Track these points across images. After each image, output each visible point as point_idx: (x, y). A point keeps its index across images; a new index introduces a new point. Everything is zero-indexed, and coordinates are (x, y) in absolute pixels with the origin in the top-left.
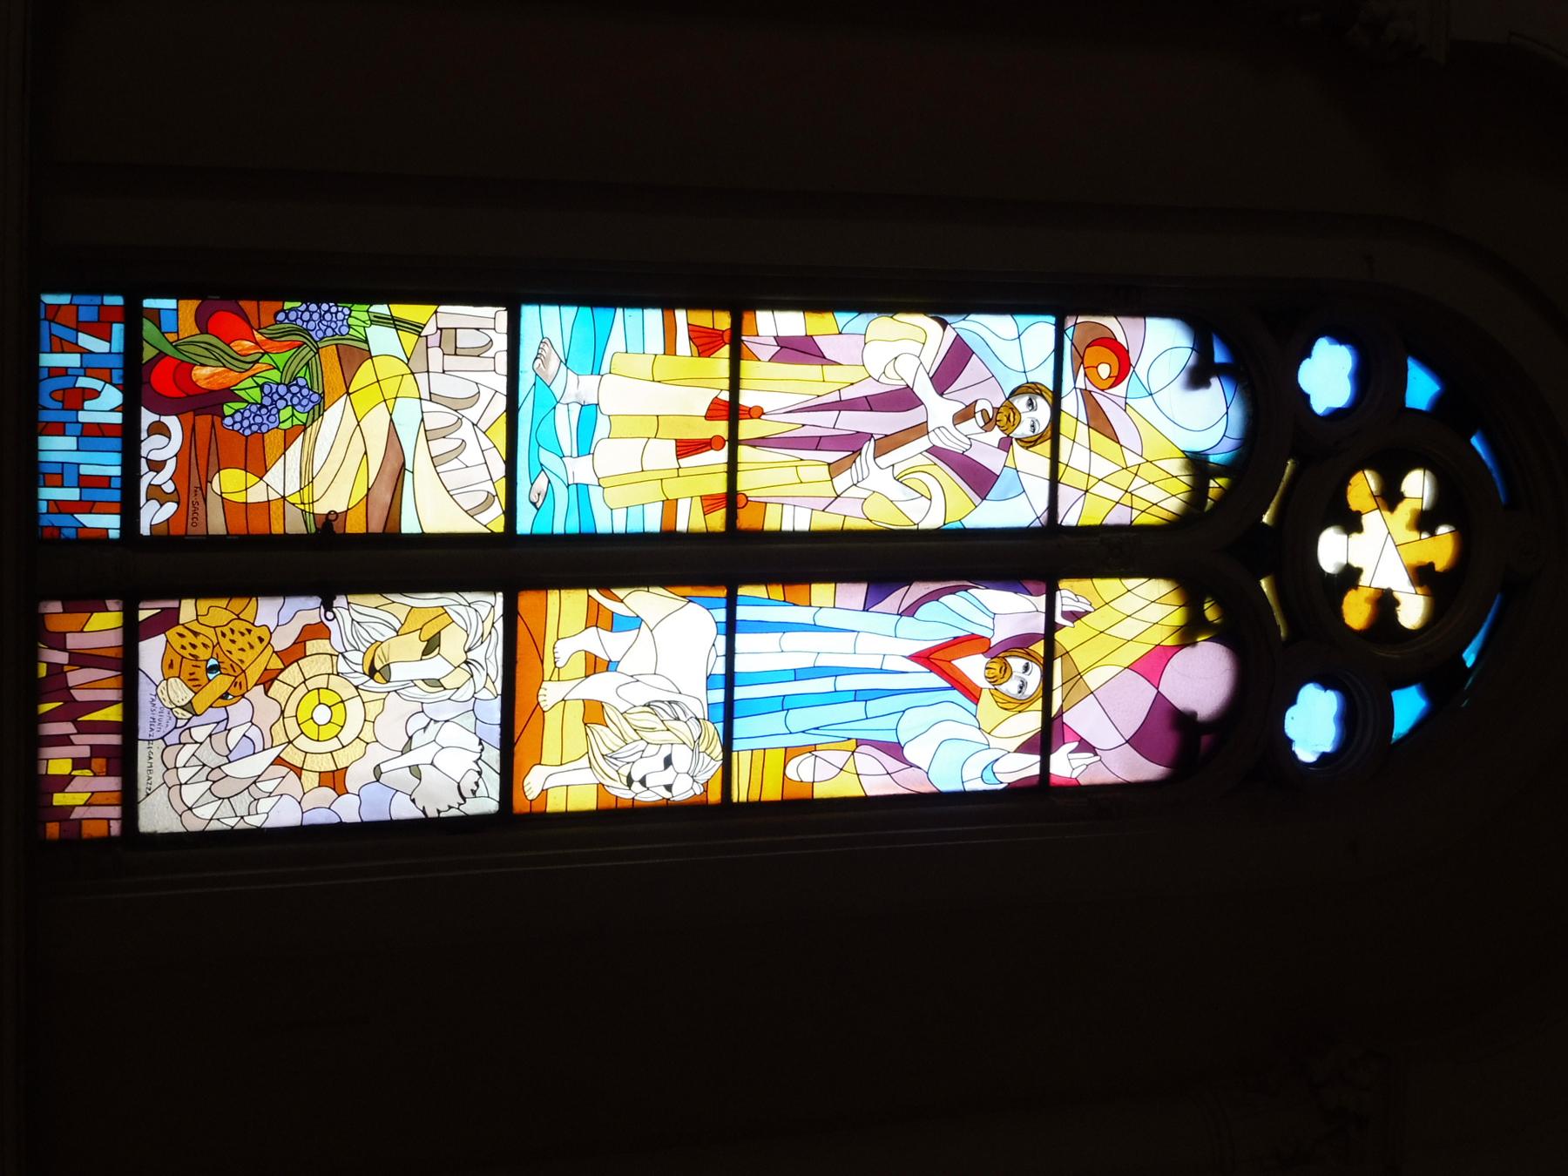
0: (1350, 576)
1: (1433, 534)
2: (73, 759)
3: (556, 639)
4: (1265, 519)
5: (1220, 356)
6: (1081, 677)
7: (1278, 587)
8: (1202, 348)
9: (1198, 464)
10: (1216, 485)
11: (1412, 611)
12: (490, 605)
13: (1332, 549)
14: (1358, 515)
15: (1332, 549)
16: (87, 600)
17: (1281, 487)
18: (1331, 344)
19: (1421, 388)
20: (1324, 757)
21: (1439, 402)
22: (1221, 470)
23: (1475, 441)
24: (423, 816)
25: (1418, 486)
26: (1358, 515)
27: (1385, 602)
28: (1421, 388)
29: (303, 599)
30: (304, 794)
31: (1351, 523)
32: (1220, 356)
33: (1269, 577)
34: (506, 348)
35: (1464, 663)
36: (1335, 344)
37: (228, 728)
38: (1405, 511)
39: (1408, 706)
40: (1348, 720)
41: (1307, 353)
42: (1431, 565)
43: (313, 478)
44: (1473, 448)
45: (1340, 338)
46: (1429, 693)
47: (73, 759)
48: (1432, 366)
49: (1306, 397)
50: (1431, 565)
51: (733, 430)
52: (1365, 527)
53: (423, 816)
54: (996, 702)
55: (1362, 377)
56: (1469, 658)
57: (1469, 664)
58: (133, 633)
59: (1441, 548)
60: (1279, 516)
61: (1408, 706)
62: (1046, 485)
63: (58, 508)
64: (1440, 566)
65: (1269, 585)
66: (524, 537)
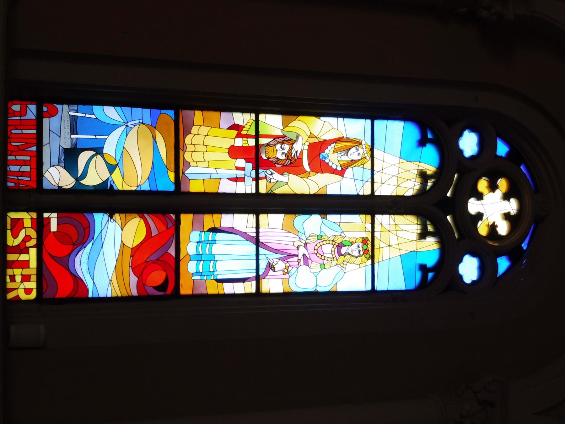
0: (479, 216)
1: (509, 200)
2: (29, 268)
4: (449, 194)
5: (430, 136)
7: (454, 219)
8: (424, 227)
9: (423, 175)
10: (430, 275)
11: (503, 229)
12: (171, 113)
13: (473, 206)
16: (25, 100)
18: (469, 132)
19: (502, 149)
20: (473, 282)
21: (508, 154)
22: (431, 177)
23: (522, 167)
25: (502, 184)
27: (493, 187)
28: (502, 149)
31: (480, 196)
32: (430, 136)
33: (450, 215)
38: (499, 193)
39: (503, 264)
40: (482, 268)
41: (461, 261)
43: (110, 283)
46: (510, 259)
47: (29, 268)
48: (507, 142)
50: (509, 213)
51: (257, 142)
55: (481, 144)
56: (524, 246)
57: (525, 248)
58: (40, 116)
59: (512, 206)
60: (454, 193)
61: (503, 264)
62: (370, 171)
65: (450, 218)
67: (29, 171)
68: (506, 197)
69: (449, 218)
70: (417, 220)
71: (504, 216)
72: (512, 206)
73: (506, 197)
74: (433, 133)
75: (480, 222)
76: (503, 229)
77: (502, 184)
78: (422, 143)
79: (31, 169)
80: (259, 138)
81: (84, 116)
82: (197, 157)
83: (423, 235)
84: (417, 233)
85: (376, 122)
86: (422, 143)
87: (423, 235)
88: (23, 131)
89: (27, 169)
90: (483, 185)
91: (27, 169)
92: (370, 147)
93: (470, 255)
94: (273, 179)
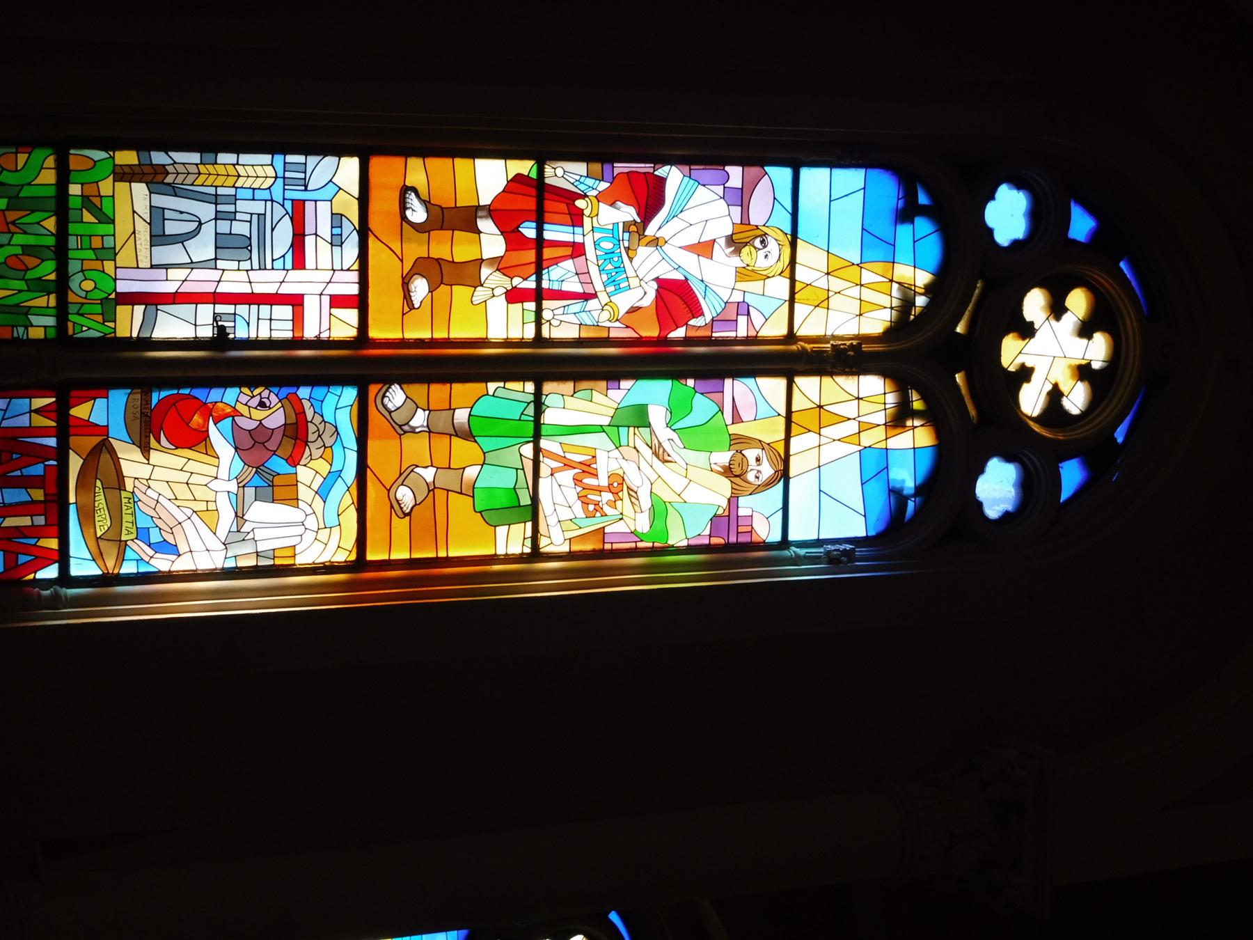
1: (1090, 337)
3: (333, 201)
4: (960, 329)
5: (923, 199)
6: (886, 423)
7: (969, 380)
8: (909, 196)
14: (1066, 310)
15: (1012, 352)
17: (974, 299)
18: (1010, 189)
21: (1095, 235)
23: (1122, 265)
24: (30, 500)
25: (1078, 302)
26: (1066, 310)
27: (1057, 309)
28: (1081, 225)
29: (369, 400)
30: (206, 485)
32: (923, 199)
34: (540, 479)
35: (1116, 440)
36: (1014, 189)
37: (432, 493)
38: (1070, 321)
39: (1071, 475)
40: (1026, 485)
41: (992, 197)
42: (1089, 365)
44: (1121, 270)
45: (1019, 185)
48: (1090, 209)
49: (990, 232)
50: (1089, 365)
52: (1061, 321)
53: (30, 500)
54: (638, 500)
55: (1035, 215)
56: (1120, 435)
57: (1120, 440)
59: (1097, 350)
60: (971, 326)
61: (1071, 475)
63: (96, 256)
64: (1096, 365)
66: (350, 153)
67: (42, 474)
68: (1085, 330)
69: (959, 378)
70: (898, 183)
71: (1077, 371)
72: (1097, 350)
73: (1085, 330)
74: (930, 193)
75: (1025, 386)
76: (1076, 399)
77: (1078, 302)
78: (906, 214)
79: (45, 495)
80: (543, 247)
81: (157, 554)
82: (410, 201)
83: (899, 419)
84: (892, 308)
85: (805, 173)
86: (906, 214)
87: (899, 419)
88: (23, 470)
89: (38, 495)
90: (1034, 304)
91: (38, 495)
92: (789, 237)
93: (1000, 459)
94: (571, 520)
